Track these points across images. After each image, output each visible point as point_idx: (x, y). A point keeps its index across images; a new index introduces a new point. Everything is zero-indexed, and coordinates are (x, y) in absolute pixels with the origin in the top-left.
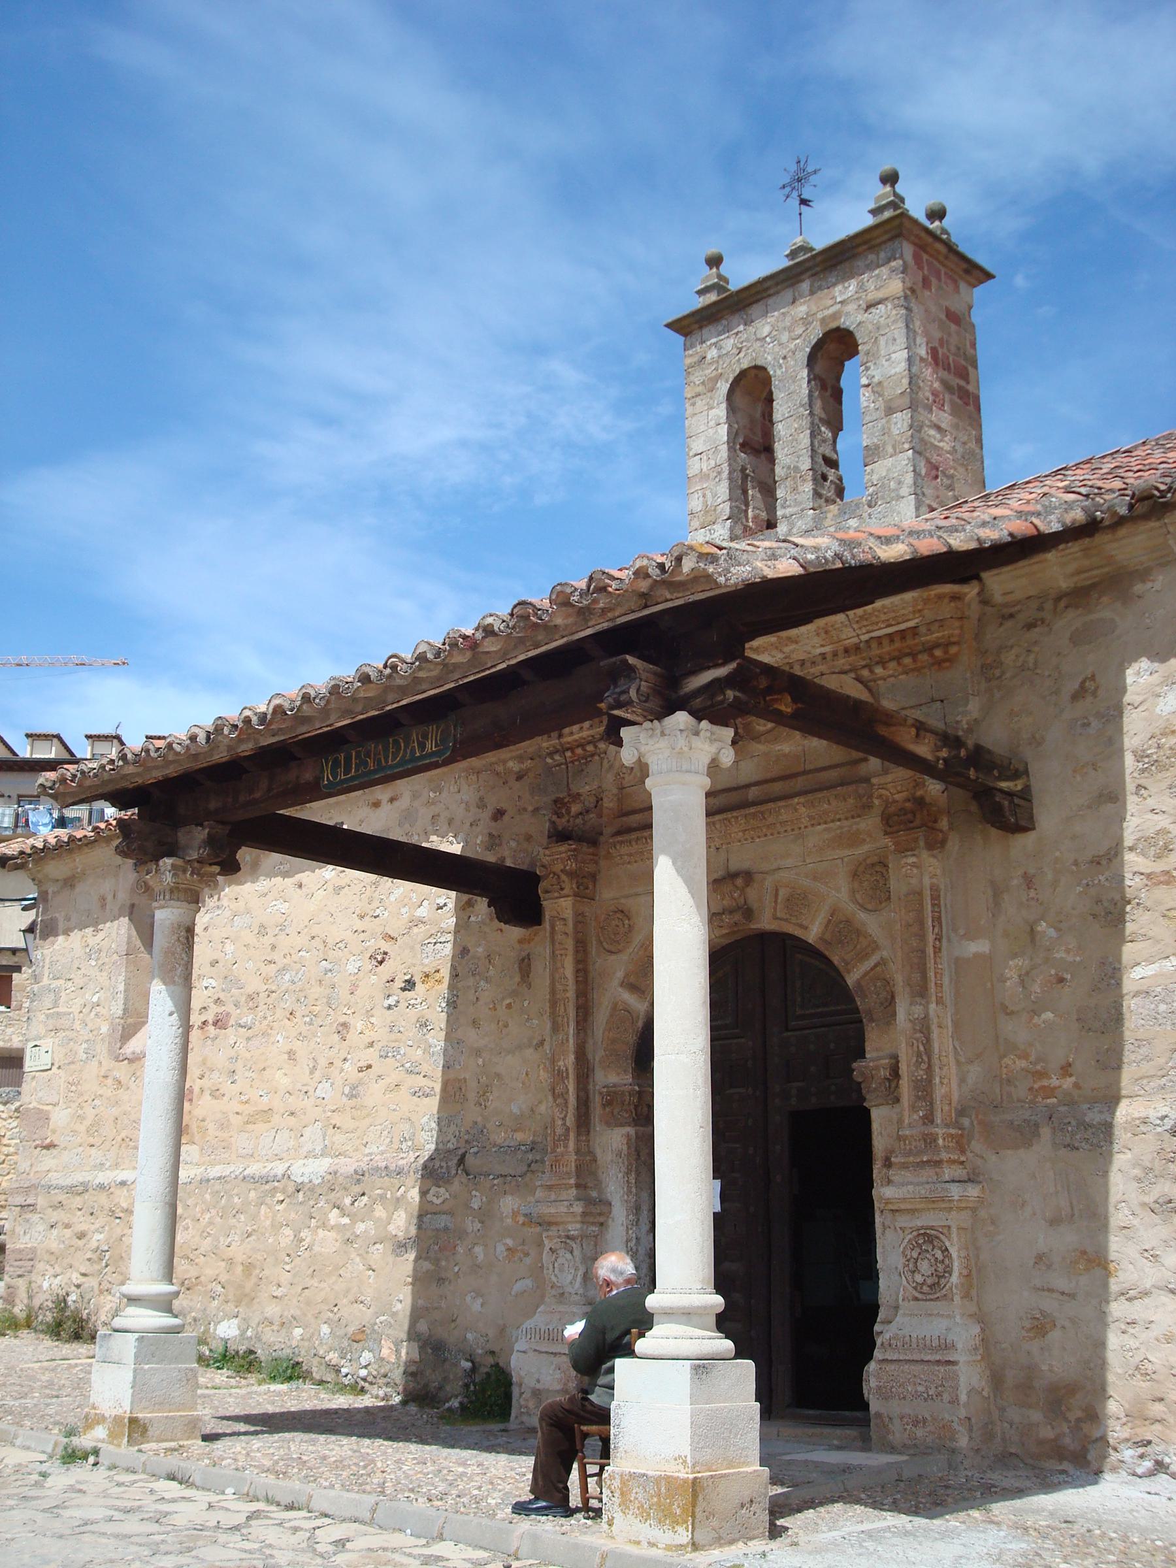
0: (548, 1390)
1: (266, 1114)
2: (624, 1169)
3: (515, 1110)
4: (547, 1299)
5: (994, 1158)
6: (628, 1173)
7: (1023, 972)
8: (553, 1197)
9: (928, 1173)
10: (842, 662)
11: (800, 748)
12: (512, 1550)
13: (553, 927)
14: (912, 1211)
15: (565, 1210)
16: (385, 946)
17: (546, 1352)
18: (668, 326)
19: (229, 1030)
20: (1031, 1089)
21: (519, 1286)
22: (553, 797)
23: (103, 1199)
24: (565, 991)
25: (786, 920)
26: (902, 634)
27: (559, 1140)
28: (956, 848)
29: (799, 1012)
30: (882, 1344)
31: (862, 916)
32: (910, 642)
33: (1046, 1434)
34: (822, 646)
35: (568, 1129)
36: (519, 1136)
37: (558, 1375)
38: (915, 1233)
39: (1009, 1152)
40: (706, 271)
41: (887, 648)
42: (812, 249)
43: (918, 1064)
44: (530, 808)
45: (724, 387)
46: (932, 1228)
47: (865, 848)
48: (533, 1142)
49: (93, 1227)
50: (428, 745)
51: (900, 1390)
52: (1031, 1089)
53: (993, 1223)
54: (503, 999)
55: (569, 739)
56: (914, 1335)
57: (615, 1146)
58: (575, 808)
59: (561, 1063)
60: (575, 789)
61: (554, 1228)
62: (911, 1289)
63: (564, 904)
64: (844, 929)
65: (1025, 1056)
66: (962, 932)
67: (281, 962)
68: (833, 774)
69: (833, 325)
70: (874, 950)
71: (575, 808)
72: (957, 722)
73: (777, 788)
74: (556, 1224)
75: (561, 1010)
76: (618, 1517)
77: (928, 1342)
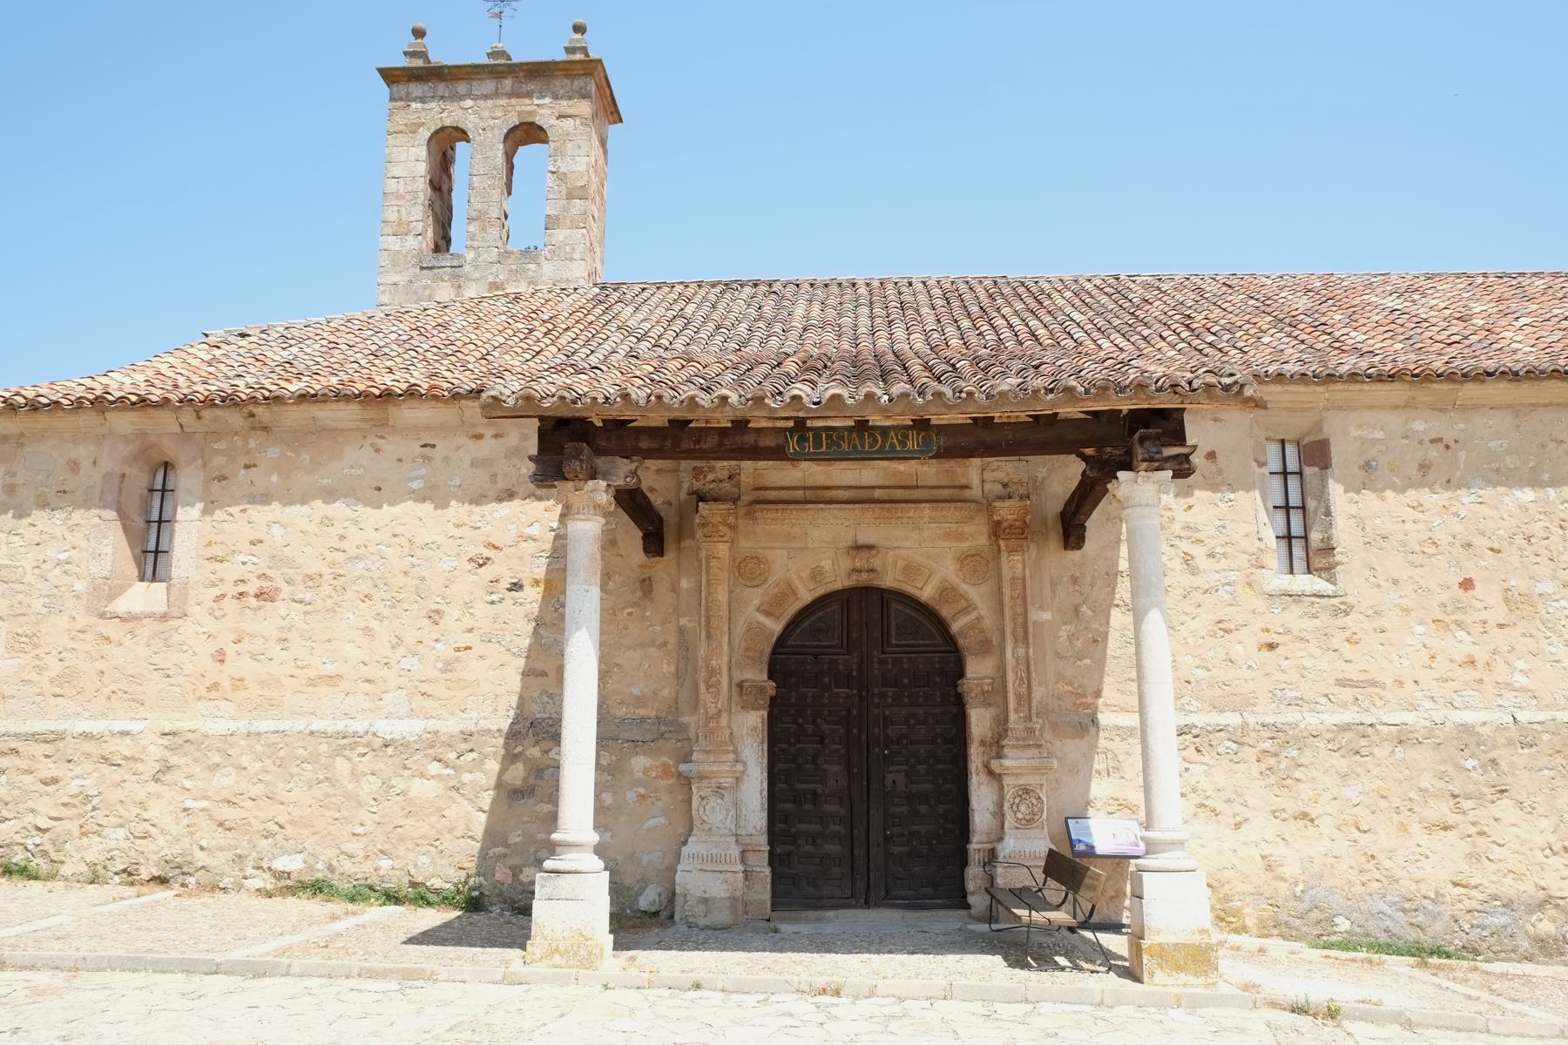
1: (333, 680)
3: (636, 692)
9: (1033, 752)
12: (1098, 1000)
13: (708, 563)
16: (487, 553)
18: (381, 71)
19: (278, 604)
21: (651, 823)
23: (90, 747)
31: (964, 587)
33: (1069, 909)
36: (642, 712)
37: (725, 886)
40: (412, 39)
42: (509, 58)
43: (1020, 685)
45: (425, 134)
47: (968, 544)
48: (657, 717)
49: (71, 774)
50: (910, 444)
58: (710, 477)
64: (948, 592)
65: (1072, 684)
67: (353, 552)
69: (530, 119)
73: (899, 494)
75: (714, 623)
76: (1158, 973)
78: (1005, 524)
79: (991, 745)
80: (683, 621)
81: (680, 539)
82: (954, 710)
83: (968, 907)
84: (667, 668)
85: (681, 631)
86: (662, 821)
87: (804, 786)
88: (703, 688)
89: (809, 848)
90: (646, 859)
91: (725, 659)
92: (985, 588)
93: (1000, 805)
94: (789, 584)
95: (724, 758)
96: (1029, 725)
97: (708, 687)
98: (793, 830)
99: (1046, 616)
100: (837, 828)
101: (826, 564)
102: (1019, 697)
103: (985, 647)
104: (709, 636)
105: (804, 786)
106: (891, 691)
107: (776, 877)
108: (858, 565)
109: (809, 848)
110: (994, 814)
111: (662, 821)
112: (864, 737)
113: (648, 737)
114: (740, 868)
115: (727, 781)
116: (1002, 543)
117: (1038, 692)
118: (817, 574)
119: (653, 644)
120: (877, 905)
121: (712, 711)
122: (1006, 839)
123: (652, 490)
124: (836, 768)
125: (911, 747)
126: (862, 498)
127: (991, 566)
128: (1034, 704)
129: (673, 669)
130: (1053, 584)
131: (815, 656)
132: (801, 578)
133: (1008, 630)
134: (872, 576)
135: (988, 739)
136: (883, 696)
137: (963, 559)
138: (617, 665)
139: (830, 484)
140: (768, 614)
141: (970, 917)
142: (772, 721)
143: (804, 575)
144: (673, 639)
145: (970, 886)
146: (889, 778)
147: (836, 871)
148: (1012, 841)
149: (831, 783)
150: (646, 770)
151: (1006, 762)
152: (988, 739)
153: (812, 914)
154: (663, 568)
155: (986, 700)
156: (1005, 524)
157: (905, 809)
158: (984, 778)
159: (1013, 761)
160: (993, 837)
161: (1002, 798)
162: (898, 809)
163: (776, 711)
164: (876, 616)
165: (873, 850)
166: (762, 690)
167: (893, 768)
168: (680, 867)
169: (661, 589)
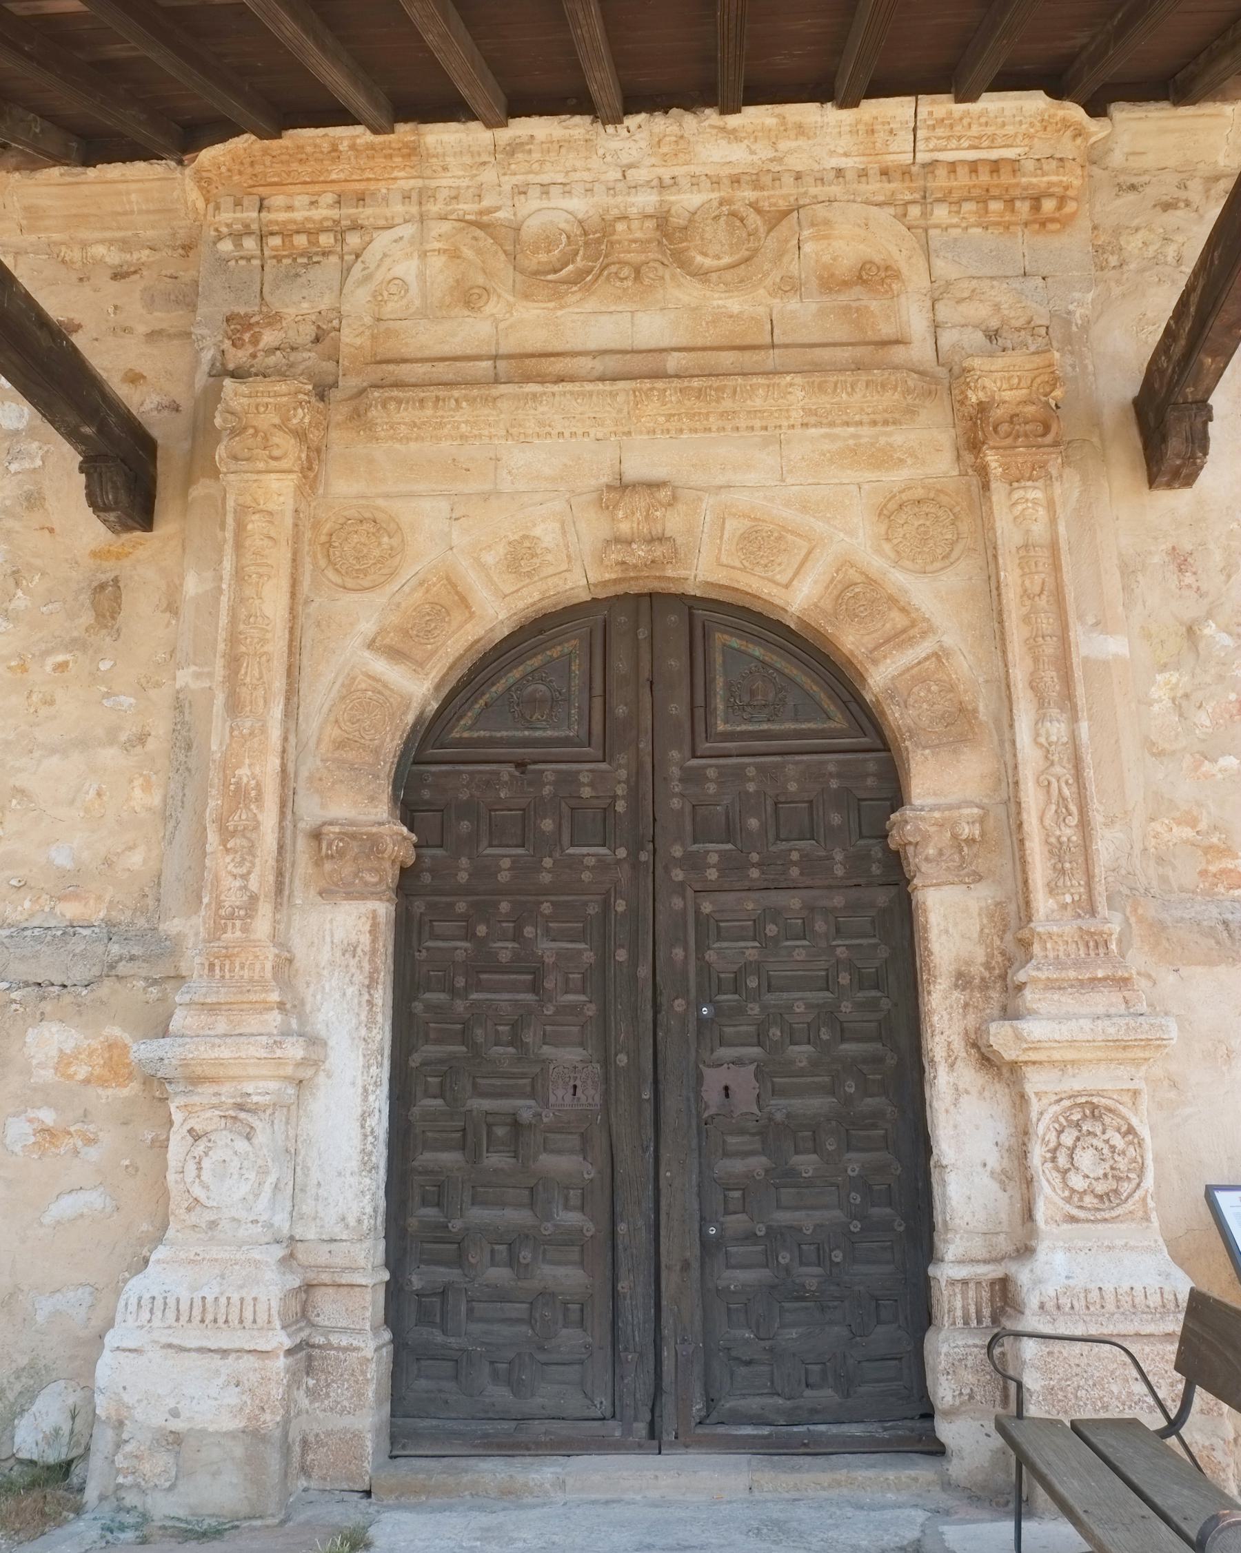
0: (203, 1433)
2: (361, 978)
3: (62, 858)
4: (170, 1233)
5: (1172, 978)
6: (371, 985)
7: (1180, 693)
8: (222, 1026)
9: (1105, 1000)
10: (876, 187)
11: (762, 311)
13: (240, 527)
14: (1063, 1066)
15: (263, 1053)
17: (200, 1350)
20: (1204, 873)
21: (66, 1206)
22: (226, 310)
24: (263, 641)
25: (744, 569)
26: (995, 166)
27: (231, 917)
28: (1076, 494)
29: (721, 727)
30: (1042, 1306)
32: (1005, 178)
34: (846, 155)
35: (254, 898)
36: (70, 910)
37: (232, 1397)
38: (1066, 1103)
39: (1199, 969)
41: (963, 178)
43: (1060, 819)
44: (142, 329)
46: (1099, 1094)
48: (109, 924)
51: (1095, 1393)
52: (1204, 873)
53: (1174, 1085)
54: (47, 653)
55: (282, 216)
56: (1109, 1288)
57: (339, 935)
58: (269, 338)
59: (244, 772)
60: (276, 304)
61: (207, 1089)
62: (1061, 1203)
63: (275, 485)
64: (858, 593)
65: (1193, 822)
66: (1090, 620)
68: (844, 354)
70: (924, 634)
71: (269, 338)
72: (1069, 313)
73: (727, 359)
74: (213, 1080)
75: (250, 672)
77: (1139, 1299)
78: (998, 413)
79: (984, 986)
80: (184, 677)
81: (188, 481)
82: (882, 897)
83: (938, 1450)
84: (145, 799)
85: (179, 704)
86: (94, 1200)
87: (487, 1104)
88: (213, 838)
89: (499, 1275)
90: (45, 1307)
91: (274, 763)
92: (959, 576)
93: (1020, 1153)
94: (451, 583)
95: (252, 1023)
96: (1090, 924)
97: (226, 834)
98: (456, 1225)
99: (1114, 646)
100: (573, 1218)
101: (547, 533)
102: (1057, 851)
103: (959, 726)
104: (234, 706)
105: (487, 1104)
106: (714, 851)
107: (405, 1358)
108: (625, 527)
109: (499, 1275)
110: (1003, 1179)
111: (94, 1200)
112: (644, 971)
113: (80, 973)
114: (283, 1340)
115: (261, 1089)
116: (992, 459)
117: (1106, 845)
118: (521, 556)
119: (111, 738)
120: (685, 1441)
121: (233, 898)
122: (1043, 1248)
123: (134, 378)
124: (571, 1055)
125: (770, 998)
126: (640, 369)
127: (964, 527)
128: (1099, 871)
129: (156, 800)
130: (1128, 571)
131: (521, 765)
132: (482, 566)
133: (1019, 676)
134: (659, 551)
135: (977, 970)
136: (694, 863)
137: (889, 511)
138: (20, 792)
139: (558, 346)
140: (395, 654)
141: (947, 1485)
142: (408, 932)
143: (489, 558)
144: (160, 727)
145: (944, 1391)
146: (714, 1079)
147: (570, 1339)
148: (1060, 1258)
149: (559, 1095)
150: (64, 1061)
151: (1034, 1029)
152: (977, 970)
153: (493, 1471)
154: (148, 556)
155: (967, 861)
156: (998, 413)
157: (758, 1164)
158: (969, 1075)
159: (1050, 1025)
160: (1004, 1244)
161: (1023, 1133)
162: (738, 1166)
163: (419, 906)
164: (676, 664)
165: (670, 1281)
166: (372, 845)
167: (724, 1053)
168: (111, 1339)
169: (141, 606)
